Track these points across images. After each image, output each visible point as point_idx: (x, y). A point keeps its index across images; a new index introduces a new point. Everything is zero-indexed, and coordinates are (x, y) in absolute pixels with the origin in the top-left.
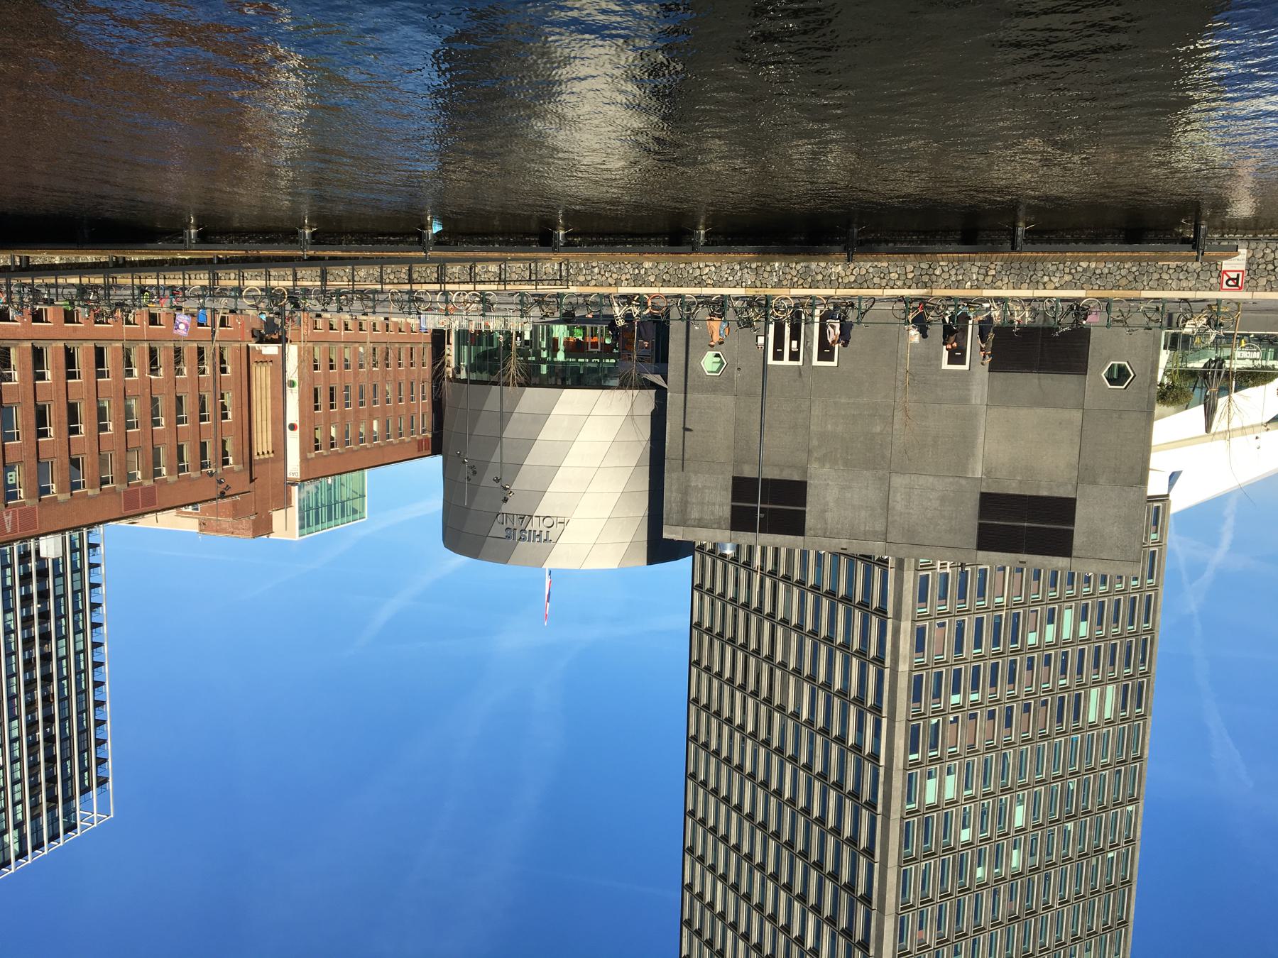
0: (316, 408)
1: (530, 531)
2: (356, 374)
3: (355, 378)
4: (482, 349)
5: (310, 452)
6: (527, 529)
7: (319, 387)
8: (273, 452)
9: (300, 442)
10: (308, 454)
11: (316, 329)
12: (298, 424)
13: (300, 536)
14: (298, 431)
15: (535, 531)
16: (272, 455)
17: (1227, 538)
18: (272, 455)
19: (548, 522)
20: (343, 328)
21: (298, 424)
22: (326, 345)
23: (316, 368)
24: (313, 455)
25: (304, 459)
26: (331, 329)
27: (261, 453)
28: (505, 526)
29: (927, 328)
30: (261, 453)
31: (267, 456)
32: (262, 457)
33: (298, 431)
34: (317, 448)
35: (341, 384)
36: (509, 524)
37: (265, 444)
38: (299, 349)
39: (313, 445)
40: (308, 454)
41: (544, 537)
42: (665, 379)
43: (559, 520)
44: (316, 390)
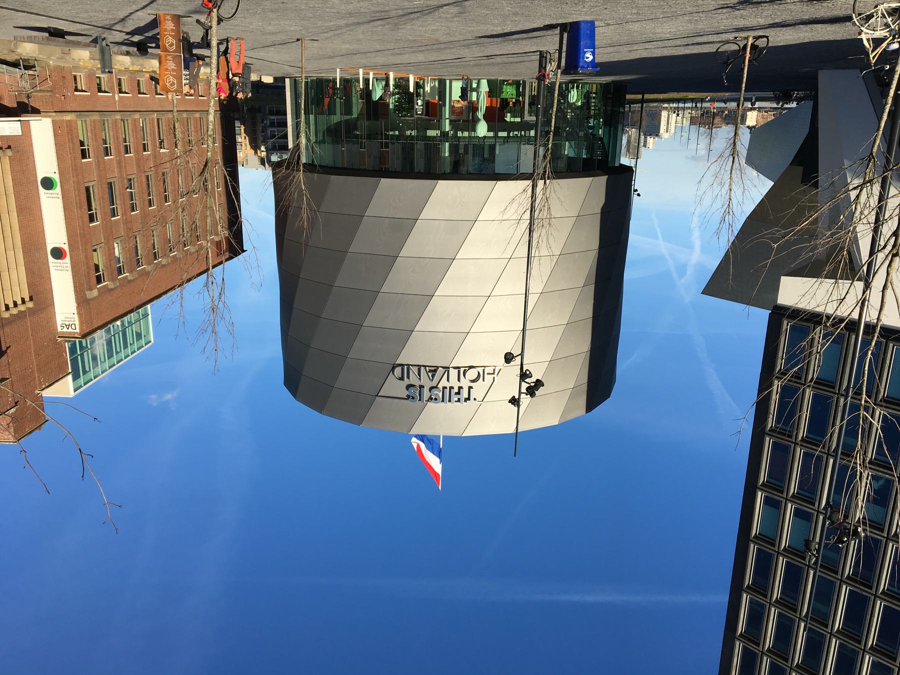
0: (92, 218)
1: (444, 388)
2: (140, 161)
3: (138, 166)
4: (336, 118)
5: (91, 290)
6: (440, 386)
7: (91, 184)
8: (31, 299)
9: (74, 277)
10: (87, 293)
11: (76, 90)
12: (66, 248)
13: (75, 390)
14: (67, 260)
15: (451, 388)
16: (30, 305)
17: (697, 244)
18: (30, 305)
19: (472, 374)
20: (116, 89)
21: (66, 248)
22: (96, 117)
23: (84, 154)
24: (95, 293)
25: (82, 302)
26: (100, 90)
27: (11, 305)
28: (406, 381)
29: (460, 97)
30: (11, 305)
31: (22, 308)
32: (14, 311)
33: (67, 260)
34: (99, 280)
35: (122, 177)
36: (414, 380)
37: (16, 289)
38: (56, 126)
39: (94, 275)
40: (87, 293)
41: (465, 394)
42: (835, 188)
43: (487, 370)
44: (87, 189)
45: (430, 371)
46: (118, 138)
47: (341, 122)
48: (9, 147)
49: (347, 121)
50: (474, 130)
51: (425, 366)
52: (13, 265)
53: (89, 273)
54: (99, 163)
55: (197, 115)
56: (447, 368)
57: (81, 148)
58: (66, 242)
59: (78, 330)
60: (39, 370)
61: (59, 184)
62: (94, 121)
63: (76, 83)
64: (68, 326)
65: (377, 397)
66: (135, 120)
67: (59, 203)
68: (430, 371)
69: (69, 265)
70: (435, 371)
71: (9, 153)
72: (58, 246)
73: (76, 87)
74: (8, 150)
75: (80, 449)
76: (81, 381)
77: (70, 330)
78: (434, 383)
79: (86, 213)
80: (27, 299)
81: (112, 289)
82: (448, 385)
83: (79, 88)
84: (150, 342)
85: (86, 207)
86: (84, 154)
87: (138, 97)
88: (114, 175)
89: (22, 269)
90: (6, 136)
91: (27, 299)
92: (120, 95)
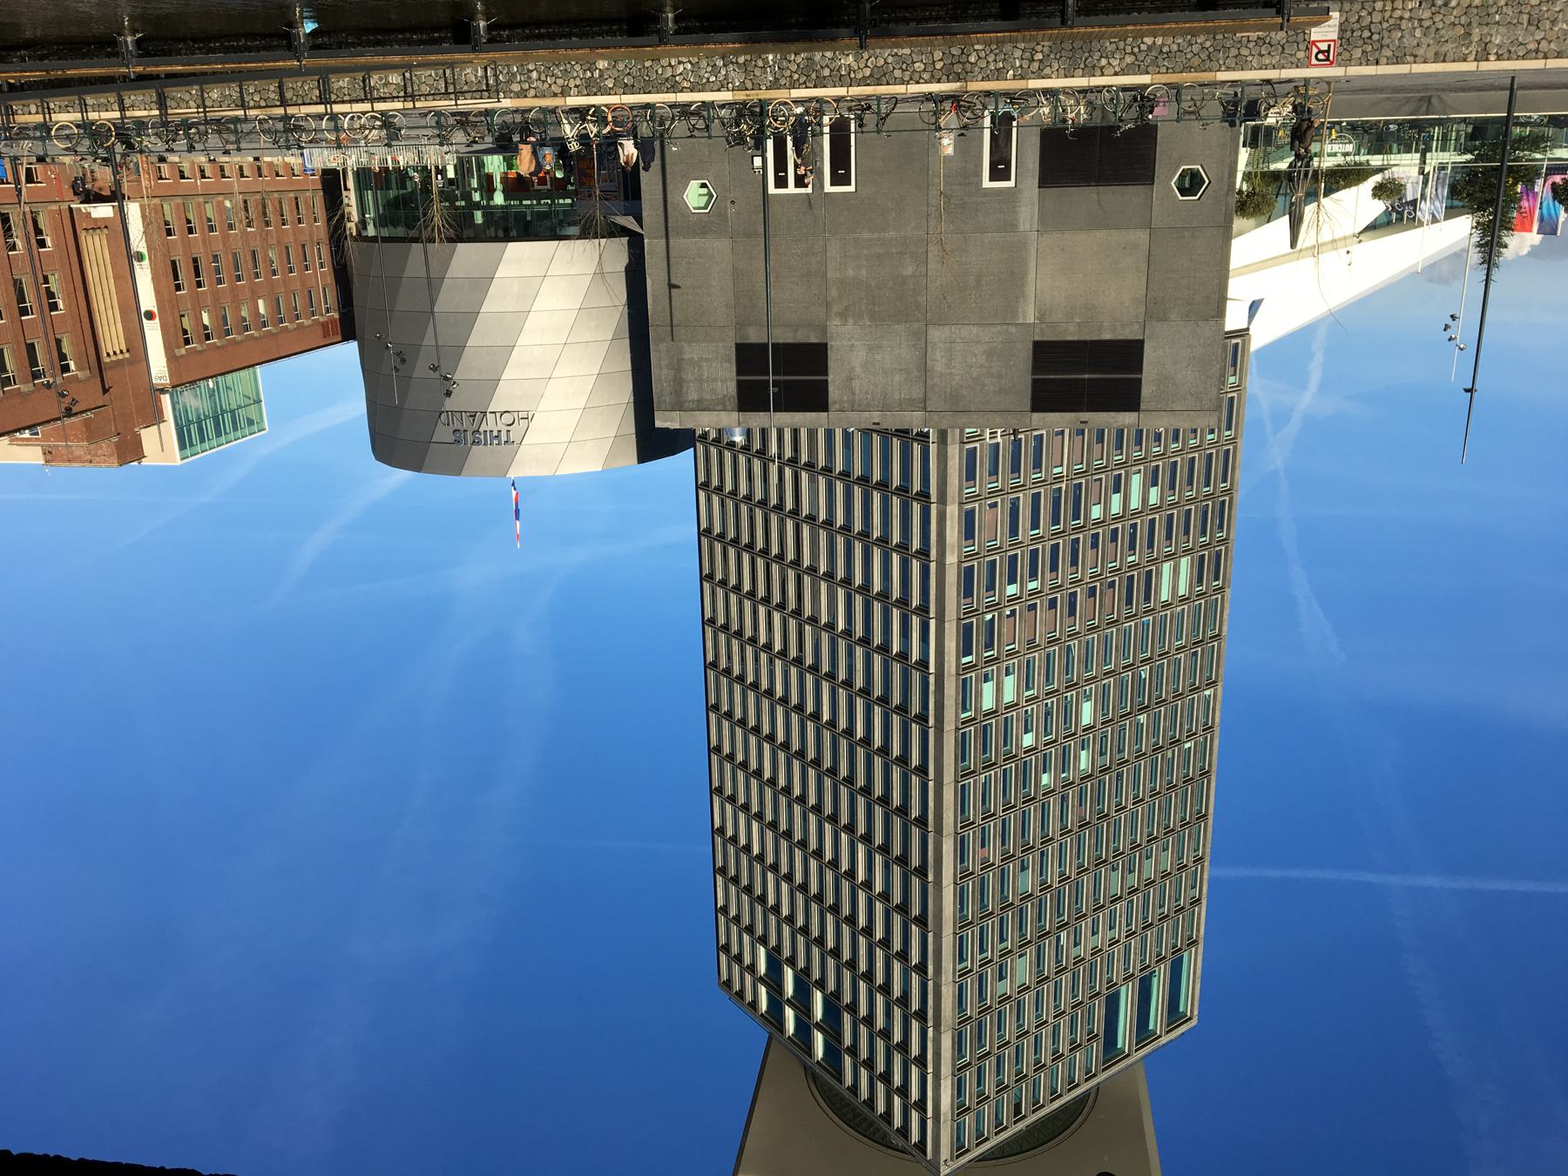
0: (178, 288)
2: (225, 238)
3: (224, 244)
4: (392, 194)
5: (179, 348)
6: (481, 430)
8: (128, 351)
10: (176, 350)
11: (161, 178)
12: (156, 310)
13: (182, 459)
16: (127, 355)
19: (507, 418)
20: (198, 175)
22: (179, 201)
24: (183, 351)
31: (120, 357)
33: (157, 319)
36: (457, 425)
40: (176, 350)
43: (521, 414)
45: (470, 416)
46: (201, 218)
47: (398, 196)
48: (106, 227)
49: (403, 194)
50: (492, 198)
51: (466, 412)
52: (112, 322)
53: (176, 334)
54: (183, 240)
55: (292, 195)
56: (485, 413)
57: (1199, 430)
58: (155, 305)
59: (168, 381)
60: (137, 412)
61: (147, 257)
62: (178, 204)
63: (160, 172)
64: (161, 378)
65: (431, 445)
66: (219, 202)
67: (148, 271)
68: (470, 416)
69: (159, 325)
70: (475, 415)
71: (106, 231)
72: (149, 309)
73: (161, 176)
74: (105, 230)
75: (163, 451)
76: (188, 452)
77: (162, 381)
78: (475, 427)
79: (172, 284)
80: (125, 351)
81: (200, 351)
82: (488, 429)
83: (164, 177)
84: (264, 429)
85: (172, 277)
86: (169, 232)
87: (180, 183)
88: (199, 252)
89: (119, 325)
90: (103, 218)
91: (125, 351)
92: (203, 180)
